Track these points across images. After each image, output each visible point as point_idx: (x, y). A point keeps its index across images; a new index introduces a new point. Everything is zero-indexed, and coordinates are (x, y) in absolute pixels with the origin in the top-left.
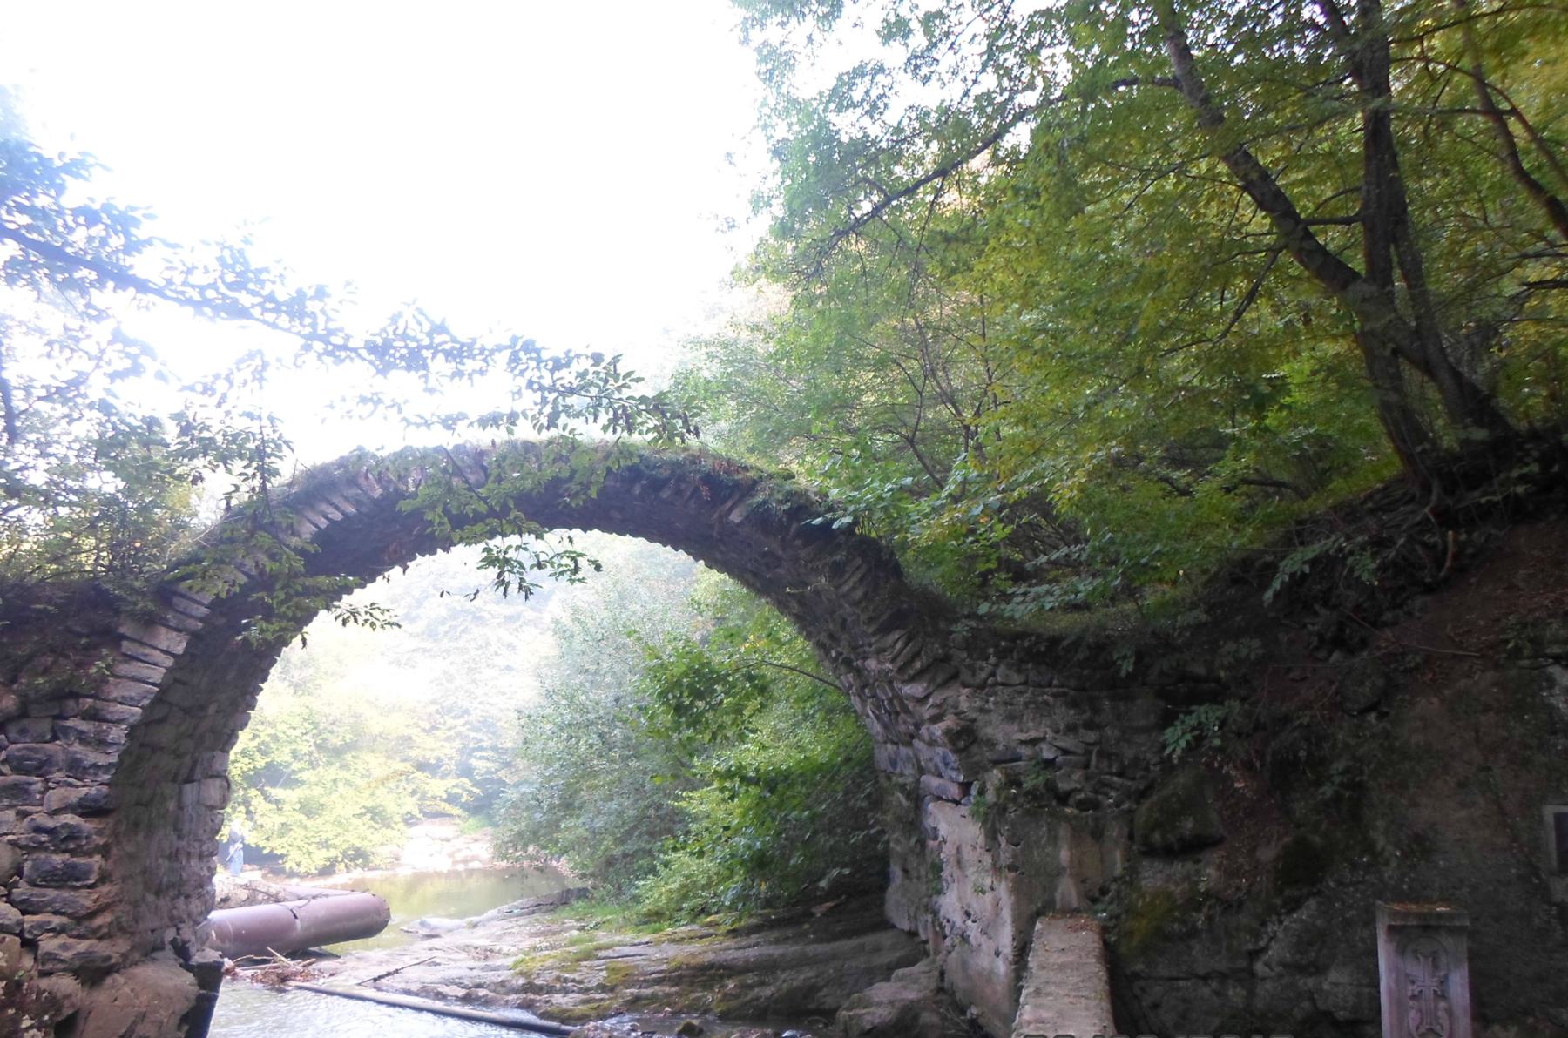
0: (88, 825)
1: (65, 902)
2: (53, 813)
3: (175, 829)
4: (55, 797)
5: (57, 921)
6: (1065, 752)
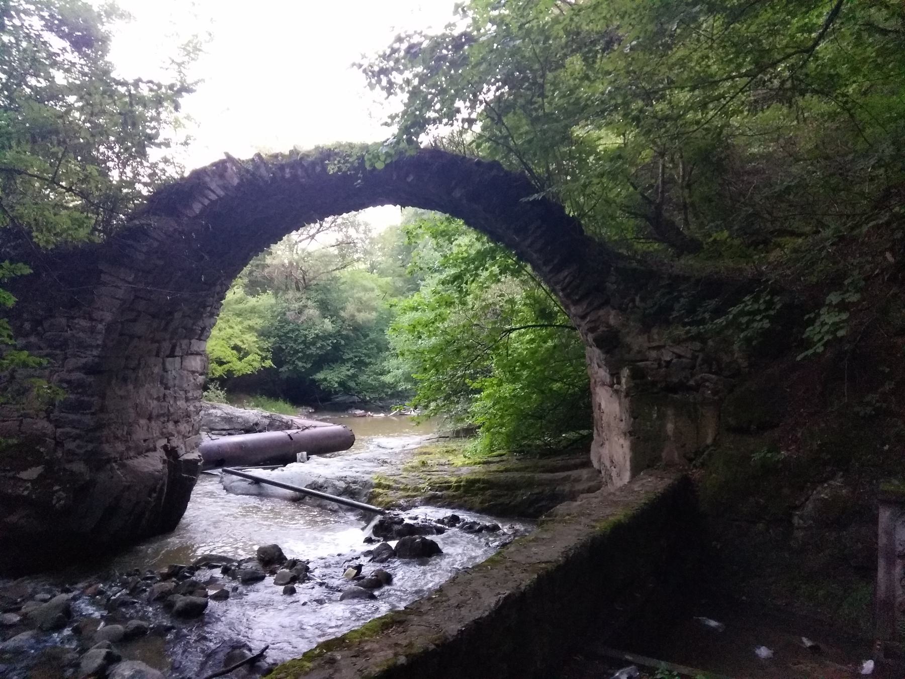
0: (91, 379)
1: (79, 421)
2: (69, 371)
3: (161, 383)
4: (71, 363)
5: (75, 432)
6: (679, 356)
